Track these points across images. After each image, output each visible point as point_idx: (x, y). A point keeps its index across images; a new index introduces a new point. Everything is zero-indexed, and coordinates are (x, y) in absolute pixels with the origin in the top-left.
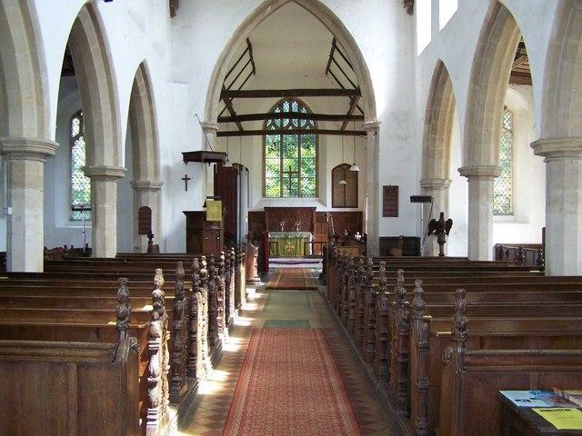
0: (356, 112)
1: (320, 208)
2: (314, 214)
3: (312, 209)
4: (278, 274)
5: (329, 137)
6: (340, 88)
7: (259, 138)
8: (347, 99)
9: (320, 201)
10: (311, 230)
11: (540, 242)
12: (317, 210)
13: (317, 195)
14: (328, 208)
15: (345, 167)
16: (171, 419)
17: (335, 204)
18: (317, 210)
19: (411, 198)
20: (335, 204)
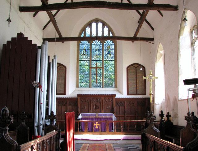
0: (145, 32)
1: (118, 96)
2: (114, 100)
3: (113, 96)
4: (85, 147)
5: (124, 42)
6: (128, 3)
7: (73, 44)
8: (134, 15)
9: (118, 91)
10: (112, 111)
11: (75, 135)
12: (117, 97)
13: (116, 87)
14: (125, 95)
15: (136, 66)
16: (192, 129)
17: (129, 93)
18: (117, 97)
19: (177, 10)
20: (129, 93)
